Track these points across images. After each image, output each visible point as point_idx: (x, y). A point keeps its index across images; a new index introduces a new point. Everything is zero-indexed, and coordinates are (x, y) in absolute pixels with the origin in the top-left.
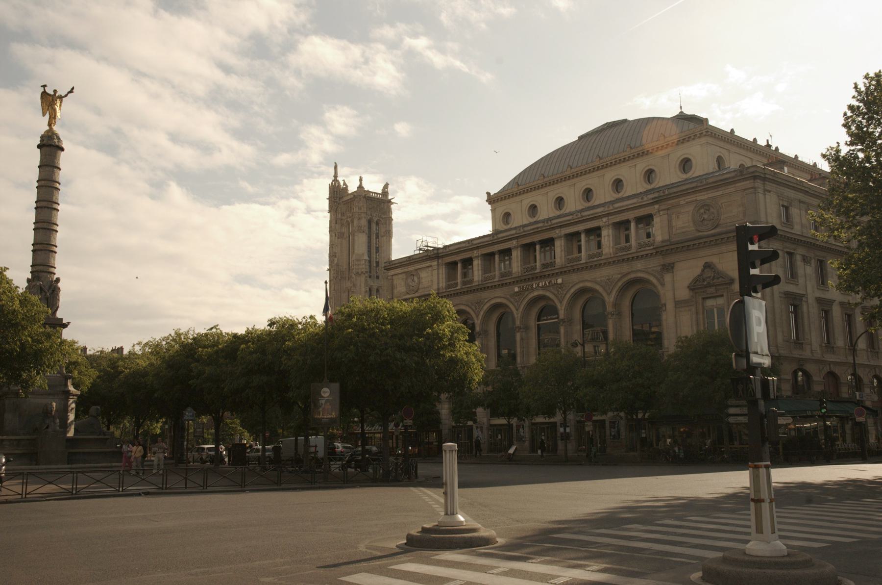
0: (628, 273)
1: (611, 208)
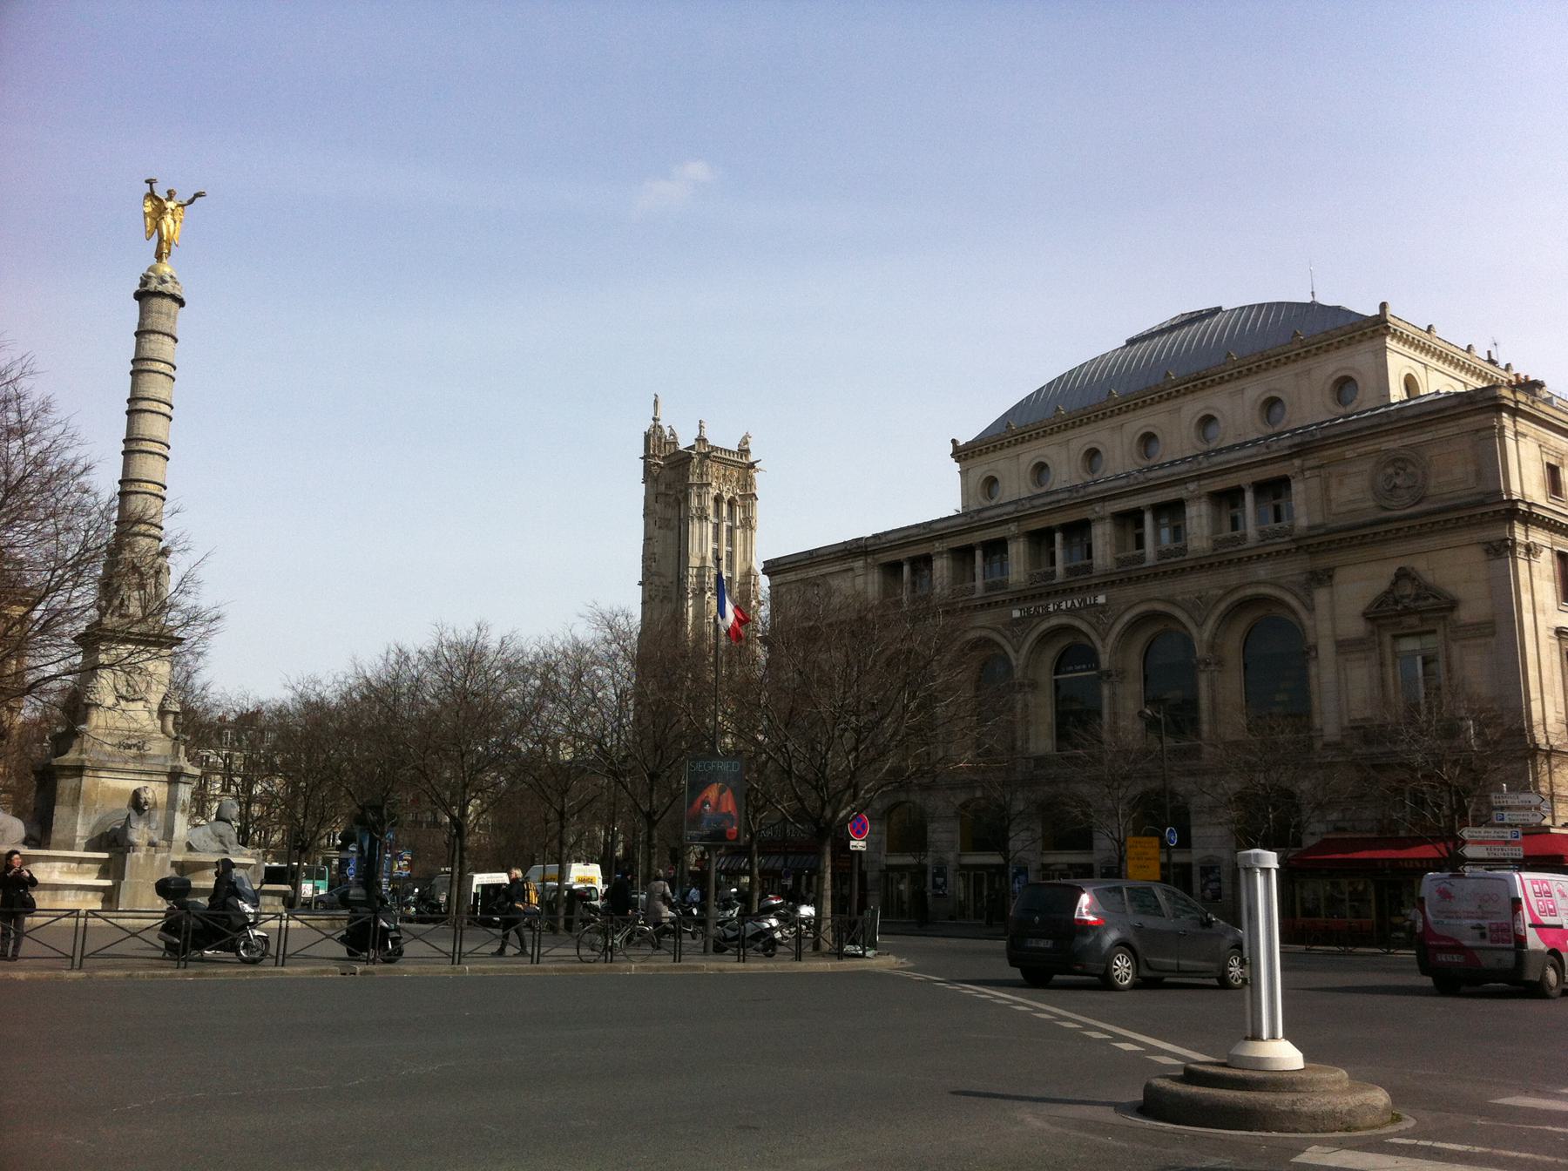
0: (1237, 588)
1: (1205, 464)
